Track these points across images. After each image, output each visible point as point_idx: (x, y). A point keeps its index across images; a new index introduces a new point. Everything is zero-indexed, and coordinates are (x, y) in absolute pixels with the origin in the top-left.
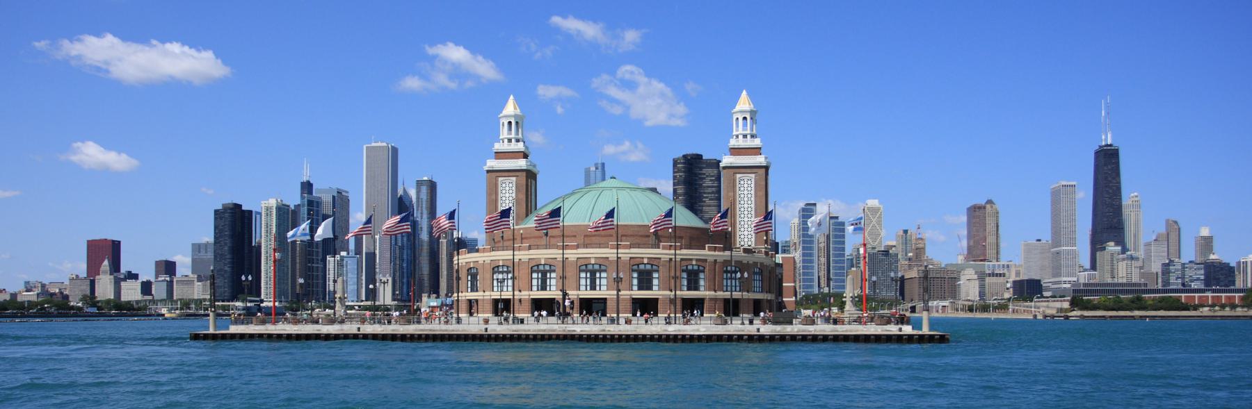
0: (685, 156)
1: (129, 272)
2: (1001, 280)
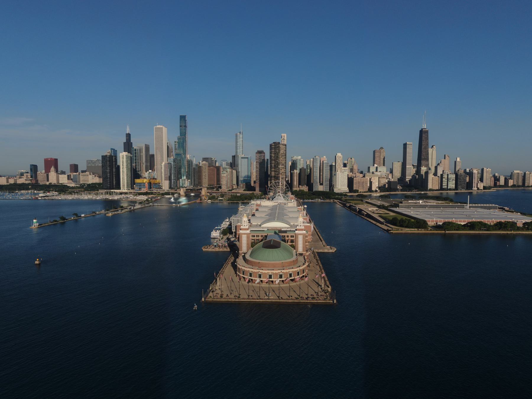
0: (274, 143)
1: (62, 171)
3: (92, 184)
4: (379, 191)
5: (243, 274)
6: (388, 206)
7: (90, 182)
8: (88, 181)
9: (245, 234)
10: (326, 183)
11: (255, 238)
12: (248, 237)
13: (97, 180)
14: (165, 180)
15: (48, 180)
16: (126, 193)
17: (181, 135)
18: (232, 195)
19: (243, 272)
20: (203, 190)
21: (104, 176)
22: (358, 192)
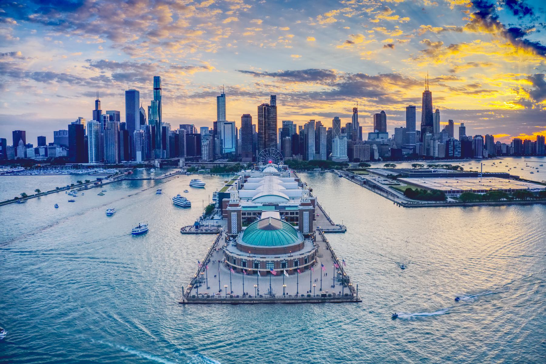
2: (387, 147)
3: (60, 157)
4: (382, 159)
5: (235, 263)
6: (397, 176)
7: (58, 155)
8: (55, 154)
9: (234, 211)
10: (323, 150)
11: (246, 216)
12: (238, 216)
13: (64, 153)
14: (255, 125)
15: (16, 155)
16: (93, 167)
17: (175, 164)
18: (214, 167)
19: (235, 261)
20: (181, 161)
21: (71, 149)
22: (359, 162)
